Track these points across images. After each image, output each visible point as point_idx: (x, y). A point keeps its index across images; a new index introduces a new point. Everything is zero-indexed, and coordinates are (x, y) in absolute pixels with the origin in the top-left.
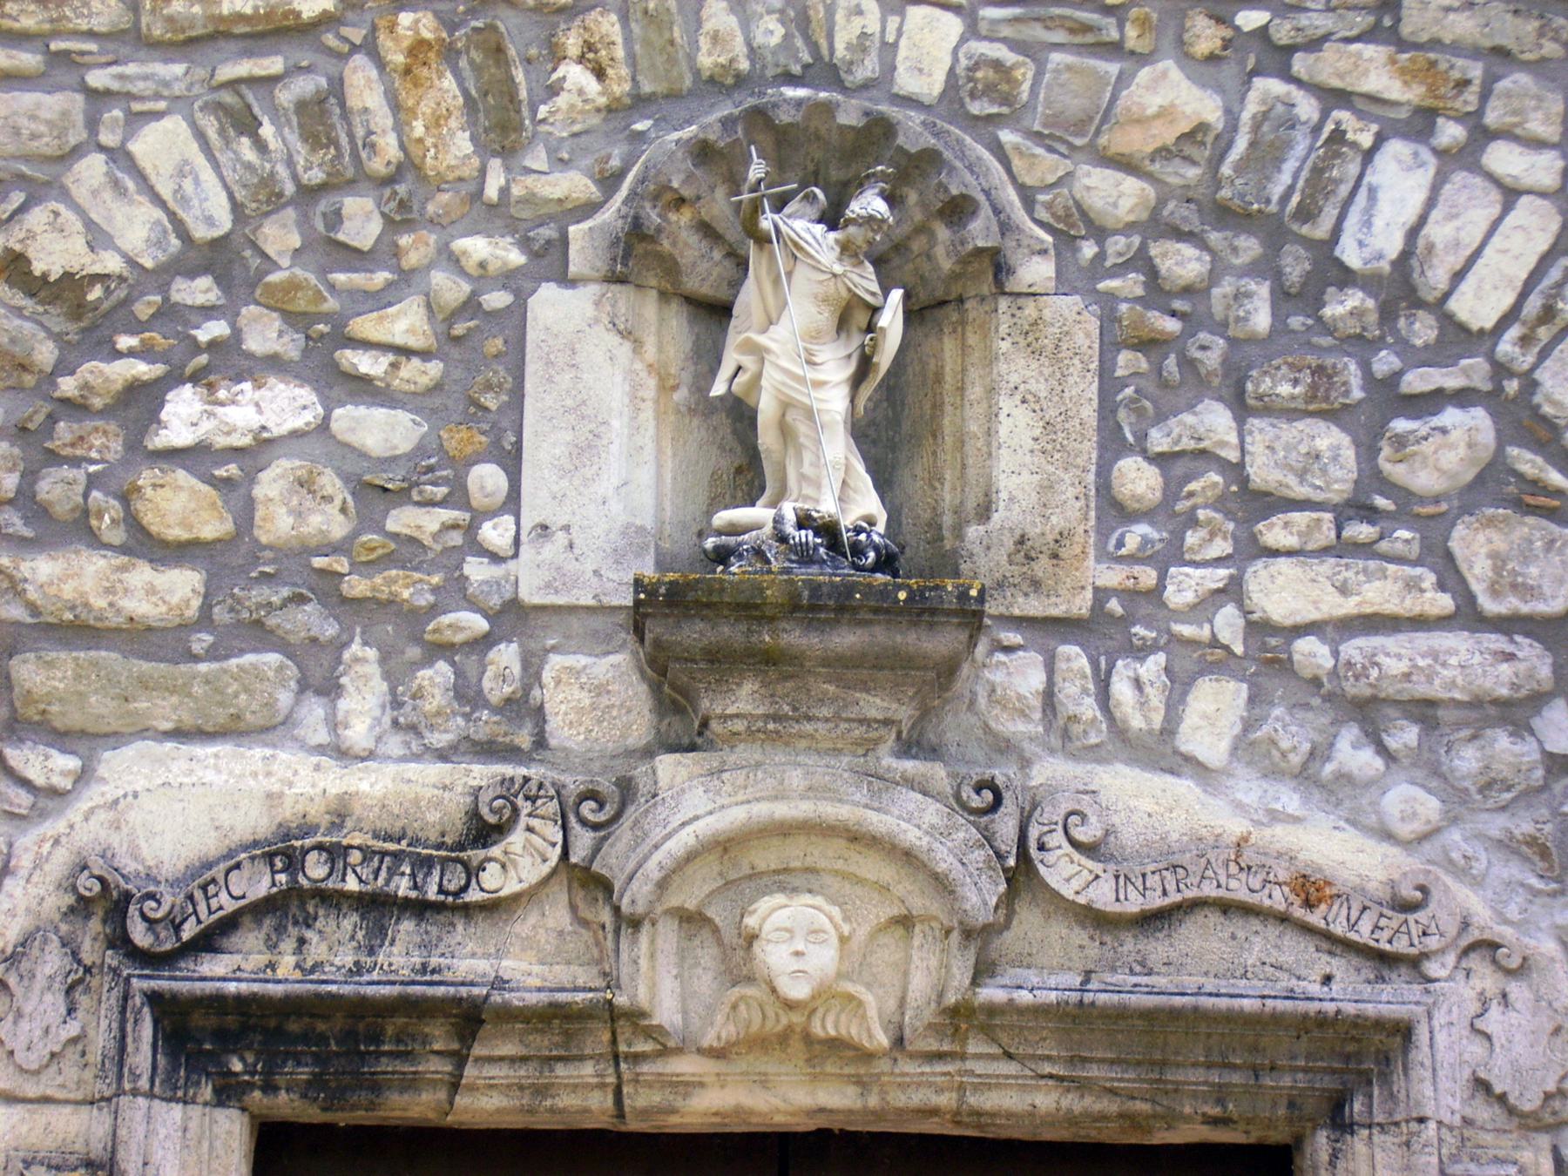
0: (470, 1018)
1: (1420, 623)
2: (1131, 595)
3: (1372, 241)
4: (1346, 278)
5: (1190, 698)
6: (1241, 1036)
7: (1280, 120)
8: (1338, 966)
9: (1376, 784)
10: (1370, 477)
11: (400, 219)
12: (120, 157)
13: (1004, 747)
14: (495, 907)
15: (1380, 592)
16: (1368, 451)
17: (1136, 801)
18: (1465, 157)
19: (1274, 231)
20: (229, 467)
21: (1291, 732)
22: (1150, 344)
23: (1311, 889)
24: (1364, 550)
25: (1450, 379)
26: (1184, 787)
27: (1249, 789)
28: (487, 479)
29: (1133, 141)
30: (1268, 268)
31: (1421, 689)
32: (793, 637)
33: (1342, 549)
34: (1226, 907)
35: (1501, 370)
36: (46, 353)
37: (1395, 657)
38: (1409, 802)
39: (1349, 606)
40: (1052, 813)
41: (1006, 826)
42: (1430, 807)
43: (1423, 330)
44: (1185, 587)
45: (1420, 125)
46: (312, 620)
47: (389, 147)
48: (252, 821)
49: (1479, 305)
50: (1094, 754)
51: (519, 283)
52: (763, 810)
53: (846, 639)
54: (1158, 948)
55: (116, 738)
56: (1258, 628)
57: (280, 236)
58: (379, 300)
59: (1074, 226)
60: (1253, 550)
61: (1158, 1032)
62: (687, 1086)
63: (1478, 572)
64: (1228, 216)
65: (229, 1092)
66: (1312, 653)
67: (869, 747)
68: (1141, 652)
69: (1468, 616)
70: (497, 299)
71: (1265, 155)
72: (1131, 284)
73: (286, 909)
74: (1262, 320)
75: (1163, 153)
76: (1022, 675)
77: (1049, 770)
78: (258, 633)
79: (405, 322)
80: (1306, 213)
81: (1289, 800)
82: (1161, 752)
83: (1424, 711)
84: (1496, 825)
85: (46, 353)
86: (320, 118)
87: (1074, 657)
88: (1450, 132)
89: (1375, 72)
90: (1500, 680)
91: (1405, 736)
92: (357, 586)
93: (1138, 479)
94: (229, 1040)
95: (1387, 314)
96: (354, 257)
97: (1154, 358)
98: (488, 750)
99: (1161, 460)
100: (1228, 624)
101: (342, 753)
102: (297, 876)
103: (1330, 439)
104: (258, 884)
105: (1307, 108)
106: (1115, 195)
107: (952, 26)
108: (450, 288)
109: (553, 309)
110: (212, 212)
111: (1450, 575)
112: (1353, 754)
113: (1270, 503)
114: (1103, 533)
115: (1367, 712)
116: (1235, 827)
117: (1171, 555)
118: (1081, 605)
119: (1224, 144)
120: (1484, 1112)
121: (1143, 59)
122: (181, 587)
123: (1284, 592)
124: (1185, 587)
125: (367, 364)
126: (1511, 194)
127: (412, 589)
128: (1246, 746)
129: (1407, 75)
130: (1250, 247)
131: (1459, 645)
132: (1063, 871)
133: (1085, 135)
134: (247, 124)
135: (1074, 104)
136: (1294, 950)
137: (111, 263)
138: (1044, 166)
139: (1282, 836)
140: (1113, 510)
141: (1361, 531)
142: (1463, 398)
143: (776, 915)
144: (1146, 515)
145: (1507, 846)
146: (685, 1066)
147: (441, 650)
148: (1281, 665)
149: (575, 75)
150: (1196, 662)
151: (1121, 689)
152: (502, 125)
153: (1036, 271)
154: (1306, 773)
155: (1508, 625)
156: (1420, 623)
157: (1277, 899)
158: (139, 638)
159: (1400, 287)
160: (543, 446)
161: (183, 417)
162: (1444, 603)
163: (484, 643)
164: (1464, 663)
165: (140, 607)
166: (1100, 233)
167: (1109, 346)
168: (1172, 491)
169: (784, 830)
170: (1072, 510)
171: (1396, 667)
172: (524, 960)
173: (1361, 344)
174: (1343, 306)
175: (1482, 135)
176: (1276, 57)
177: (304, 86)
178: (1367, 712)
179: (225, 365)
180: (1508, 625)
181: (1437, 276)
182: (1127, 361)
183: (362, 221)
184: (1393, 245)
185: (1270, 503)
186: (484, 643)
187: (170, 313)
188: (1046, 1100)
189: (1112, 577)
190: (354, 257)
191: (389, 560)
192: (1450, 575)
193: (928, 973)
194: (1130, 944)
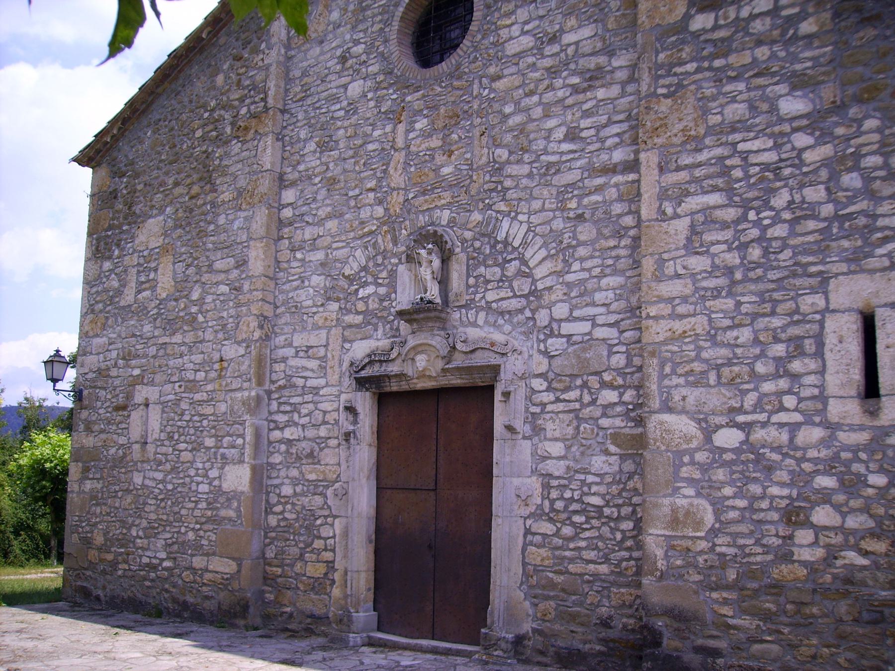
0: (389, 377)
1: (508, 298)
2: (471, 300)
3: (501, 236)
4: (499, 242)
5: (815, 200)
6: (481, 369)
7: (490, 217)
8: (497, 356)
9: (503, 325)
10: (503, 275)
11: (384, 258)
12: (354, 256)
13: (454, 327)
14: (393, 360)
15: (503, 294)
16: (502, 270)
17: (473, 333)
18: (514, 219)
19: (489, 236)
20: (365, 299)
21: (491, 319)
22: (473, 259)
23: (493, 344)
24: (501, 287)
25: (513, 257)
26: (478, 330)
27: (486, 329)
28: (393, 295)
29: (470, 226)
30: (489, 243)
31: (509, 309)
32: (416, 316)
33: (498, 288)
34: (482, 348)
35: (519, 253)
36: (346, 287)
37: (504, 305)
38: (508, 328)
39: (498, 297)
40: (458, 337)
41: (451, 340)
42: (510, 328)
43: (510, 249)
44: (478, 296)
45: (509, 215)
46: (375, 320)
47: (382, 247)
48: (368, 351)
49: (516, 244)
50: (466, 326)
51: (397, 265)
52: (419, 342)
53: (422, 316)
54: (473, 356)
55: (354, 341)
56: (487, 302)
57: (371, 264)
58: (382, 271)
59: (464, 241)
60: (487, 290)
61: (469, 370)
62: (416, 384)
63: (516, 288)
64: (483, 235)
65: (367, 390)
66: (494, 305)
67: (433, 330)
68: (472, 309)
69: (515, 296)
70: (395, 268)
71: (488, 224)
72: (471, 249)
73: (371, 363)
74: (488, 251)
75: (474, 227)
76: (456, 315)
77: (461, 329)
78: (369, 323)
79: (384, 274)
80: (493, 233)
81: (492, 330)
82: (474, 324)
83: (509, 312)
84: (519, 330)
85: (346, 287)
86: (375, 246)
87: (463, 311)
88: (513, 214)
89: (502, 206)
90: (519, 306)
91: (507, 317)
92: (379, 315)
93: (472, 281)
94: (366, 382)
95: (505, 247)
96: (379, 265)
97: (475, 261)
98: (394, 337)
99: (475, 277)
100: (483, 303)
101: (378, 340)
102: (372, 359)
103: (497, 270)
104: (367, 360)
105: (494, 214)
106: (468, 235)
107: (449, 211)
108: (389, 267)
109: (401, 268)
110: (363, 263)
111: (513, 290)
112: (501, 321)
113: (488, 282)
114: (467, 291)
115: (502, 314)
116: (484, 335)
117: (475, 293)
118: (464, 303)
119: (482, 223)
120: (515, 377)
121: (473, 211)
122: (361, 317)
123: (491, 296)
124: (478, 296)
125: (380, 281)
126: (521, 223)
127: (385, 314)
128: (486, 322)
129: (507, 206)
130: (487, 239)
131: (513, 301)
132: (459, 346)
133: (464, 227)
134: (367, 248)
135: (463, 222)
136: (492, 354)
137: (353, 272)
138: (459, 232)
139: (490, 336)
140: (468, 286)
141: (501, 284)
142: (515, 259)
143: (419, 358)
144: (473, 287)
145: (521, 333)
146: (415, 381)
147: (389, 322)
148: (490, 308)
149: (404, 231)
150: (479, 309)
151: (469, 315)
152: (395, 242)
153: (458, 250)
154: (495, 325)
155: (520, 296)
156: (508, 298)
157: (487, 346)
158: (358, 326)
159: (506, 243)
160: (399, 290)
161: (361, 293)
162: (512, 294)
163: (393, 320)
164: (514, 304)
165: (356, 322)
166: (467, 241)
167: (468, 260)
168: (477, 282)
169: (421, 345)
170: (463, 288)
171: (504, 306)
172: (394, 368)
173: (502, 253)
174: (499, 246)
175: (517, 214)
176: (490, 207)
177: (373, 241)
178: (502, 314)
179: (365, 284)
180: (520, 296)
181: (510, 240)
182: (471, 262)
183: (380, 260)
184: (504, 235)
185: (488, 282)
186: (393, 320)
187: (360, 278)
188: (459, 381)
189: (468, 297)
190: (379, 265)
191: (383, 310)
192: (513, 290)
193: (440, 364)
194: (469, 356)
